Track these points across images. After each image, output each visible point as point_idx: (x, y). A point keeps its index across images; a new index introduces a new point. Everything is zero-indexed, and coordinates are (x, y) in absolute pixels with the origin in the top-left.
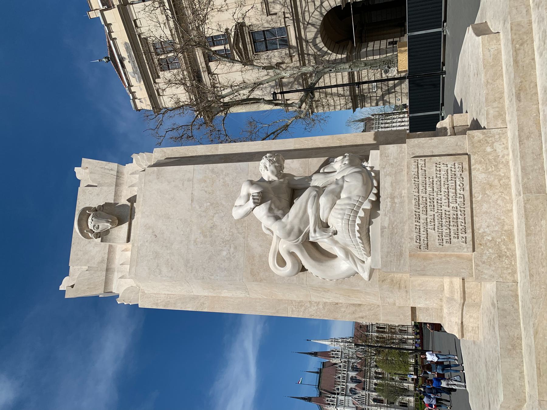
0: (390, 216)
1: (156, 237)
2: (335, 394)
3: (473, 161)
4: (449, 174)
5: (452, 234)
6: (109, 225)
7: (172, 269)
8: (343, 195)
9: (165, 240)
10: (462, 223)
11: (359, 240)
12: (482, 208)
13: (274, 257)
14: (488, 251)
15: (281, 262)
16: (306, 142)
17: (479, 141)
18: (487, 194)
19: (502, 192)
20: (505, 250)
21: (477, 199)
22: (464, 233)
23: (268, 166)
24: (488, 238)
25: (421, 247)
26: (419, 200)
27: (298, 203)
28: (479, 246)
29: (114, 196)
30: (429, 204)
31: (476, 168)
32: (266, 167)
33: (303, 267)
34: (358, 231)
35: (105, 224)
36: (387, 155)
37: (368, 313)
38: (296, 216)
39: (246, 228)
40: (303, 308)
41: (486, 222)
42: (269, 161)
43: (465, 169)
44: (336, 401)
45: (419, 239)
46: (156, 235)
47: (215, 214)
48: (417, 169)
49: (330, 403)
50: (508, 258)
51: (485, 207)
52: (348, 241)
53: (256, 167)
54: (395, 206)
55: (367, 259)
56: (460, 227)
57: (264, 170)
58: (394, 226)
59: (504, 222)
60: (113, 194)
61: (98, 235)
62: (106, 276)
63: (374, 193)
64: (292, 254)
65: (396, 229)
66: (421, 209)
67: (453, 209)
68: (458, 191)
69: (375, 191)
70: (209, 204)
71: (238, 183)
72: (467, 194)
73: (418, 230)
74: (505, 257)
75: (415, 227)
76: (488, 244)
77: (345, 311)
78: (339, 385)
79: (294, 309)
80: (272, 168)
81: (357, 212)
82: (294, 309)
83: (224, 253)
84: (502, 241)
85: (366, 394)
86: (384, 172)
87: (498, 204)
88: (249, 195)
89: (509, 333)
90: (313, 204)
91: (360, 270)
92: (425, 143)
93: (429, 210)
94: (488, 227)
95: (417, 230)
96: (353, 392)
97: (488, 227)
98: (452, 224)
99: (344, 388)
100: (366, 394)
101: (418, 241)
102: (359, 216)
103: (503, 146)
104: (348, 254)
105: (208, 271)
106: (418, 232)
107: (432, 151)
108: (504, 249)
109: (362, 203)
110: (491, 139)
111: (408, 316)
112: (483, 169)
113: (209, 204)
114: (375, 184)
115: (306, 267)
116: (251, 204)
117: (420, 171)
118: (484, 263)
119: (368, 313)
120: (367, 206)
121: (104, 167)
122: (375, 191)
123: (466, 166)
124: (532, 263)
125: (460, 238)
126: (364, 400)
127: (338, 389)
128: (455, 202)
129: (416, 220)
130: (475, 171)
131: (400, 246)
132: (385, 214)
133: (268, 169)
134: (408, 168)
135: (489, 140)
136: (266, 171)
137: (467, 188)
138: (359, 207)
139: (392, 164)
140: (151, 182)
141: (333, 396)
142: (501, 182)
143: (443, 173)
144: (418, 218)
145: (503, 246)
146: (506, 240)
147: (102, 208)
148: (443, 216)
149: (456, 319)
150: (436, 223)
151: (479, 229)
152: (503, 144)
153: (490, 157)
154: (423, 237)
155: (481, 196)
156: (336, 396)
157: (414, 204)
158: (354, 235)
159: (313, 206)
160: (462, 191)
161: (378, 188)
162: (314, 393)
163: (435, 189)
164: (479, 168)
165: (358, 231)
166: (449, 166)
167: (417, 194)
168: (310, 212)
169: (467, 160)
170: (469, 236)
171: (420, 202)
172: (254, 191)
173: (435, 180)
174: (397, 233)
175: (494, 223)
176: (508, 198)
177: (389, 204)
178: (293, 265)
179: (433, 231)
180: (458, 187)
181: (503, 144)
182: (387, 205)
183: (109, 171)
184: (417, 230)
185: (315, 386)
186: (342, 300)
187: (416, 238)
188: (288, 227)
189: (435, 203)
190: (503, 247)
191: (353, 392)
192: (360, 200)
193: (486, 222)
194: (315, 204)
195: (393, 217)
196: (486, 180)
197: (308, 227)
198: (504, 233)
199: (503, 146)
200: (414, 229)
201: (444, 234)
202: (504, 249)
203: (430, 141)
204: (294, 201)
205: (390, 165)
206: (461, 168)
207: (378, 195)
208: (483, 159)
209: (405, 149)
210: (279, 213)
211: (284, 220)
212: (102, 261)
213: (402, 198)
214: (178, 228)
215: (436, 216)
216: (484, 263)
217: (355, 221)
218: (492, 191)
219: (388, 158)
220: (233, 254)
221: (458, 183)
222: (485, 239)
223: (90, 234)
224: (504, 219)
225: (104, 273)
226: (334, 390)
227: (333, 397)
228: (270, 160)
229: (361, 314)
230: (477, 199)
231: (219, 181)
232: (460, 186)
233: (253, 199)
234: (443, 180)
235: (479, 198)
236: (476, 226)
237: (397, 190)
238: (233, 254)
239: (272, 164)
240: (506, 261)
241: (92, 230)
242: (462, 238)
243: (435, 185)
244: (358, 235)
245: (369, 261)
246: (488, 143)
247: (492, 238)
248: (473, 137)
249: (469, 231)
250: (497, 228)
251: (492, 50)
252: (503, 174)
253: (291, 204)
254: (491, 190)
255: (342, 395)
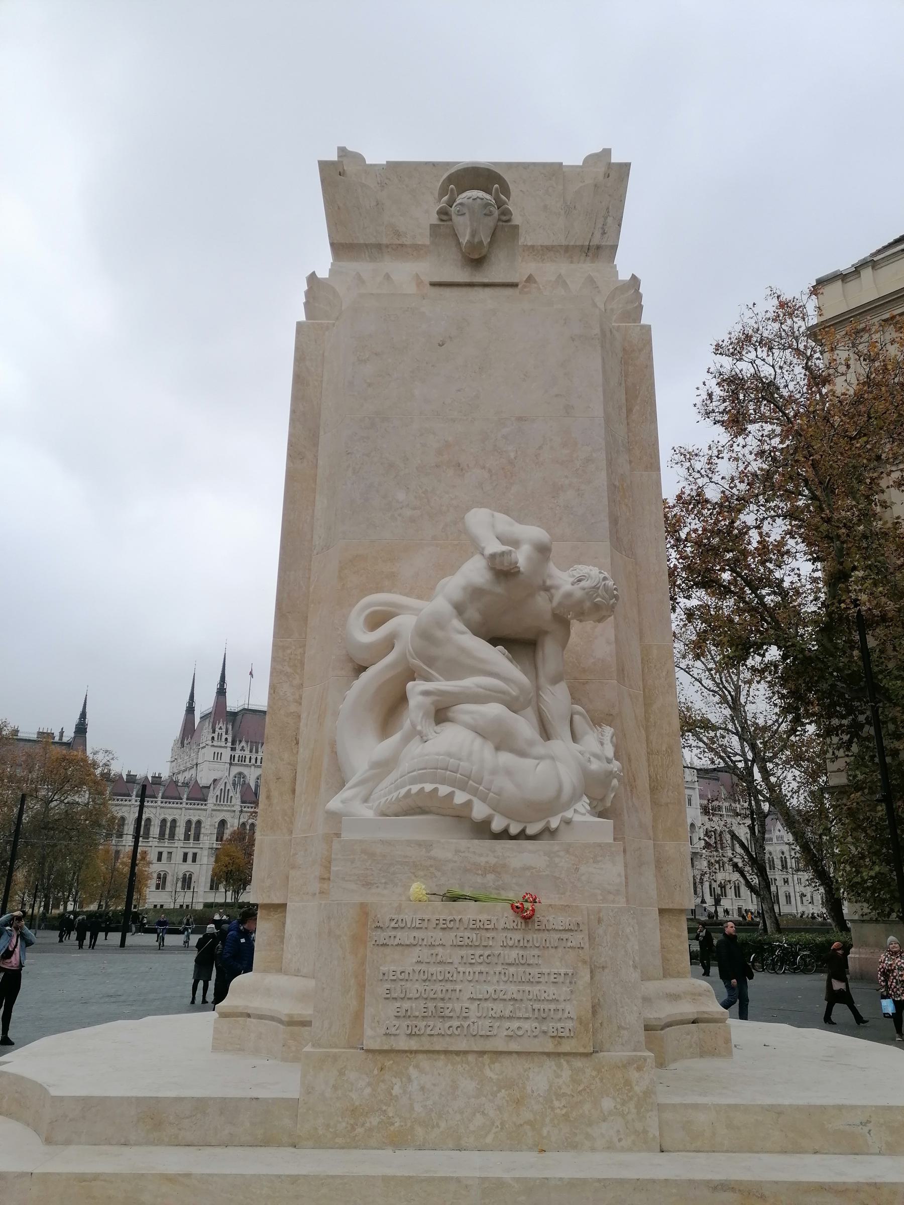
0: (455, 862)
1: (440, 345)
2: (233, 743)
3: (578, 1063)
4: (546, 1006)
5: (406, 1005)
6: (467, 238)
7: (370, 385)
8: (505, 758)
9: (433, 366)
10: (430, 1028)
11: (403, 791)
12: (466, 1079)
13: (380, 604)
14: (369, 1084)
15: (376, 620)
16: (664, 674)
17: (628, 1083)
18: (499, 1091)
19: (502, 1128)
20: (368, 1125)
21: (487, 1067)
22: (409, 1032)
23: (582, 584)
24: (396, 1088)
25: (379, 932)
26: (487, 929)
27: (496, 656)
28: (380, 1066)
29: (541, 246)
30: (479, 952)
31: (562, 1070)
32: (580, 581)
33: (364, 669)
34: (423, 788)
35: (469, 228)
36: (599, 859)
37: (278, 808)
38: (463, 650)
39: (456, 542)
40: (289, 670)
41: (434, 1085)
42: (594, 587)
43: (559, 1043)
44: (219, 744)
45: (397, 926)
46: (443, 345)
47: (490, 471)
48: (561, 928)
49: (217, 733)
50: (349, 1128)
51: (468, 1085)
52: (405, 765)
53: (596, 558)
54: (478, 874)
55: (370, 808)
56: (422, 1024)
57: (574, 576)
58: (432, 870)
59: (433, 1127)
60: (547, 243)
61: (444, 214)
62: (366, 245)
63: (508, 826)
64: (389, 644)
65: (425, 875)
66: (467, 934)
67: (464, 1010)
68: (507, 1024)
69: (514, 830)
70: (512, 455)
71: (560, 519)
72: (499, 1044)
73: (418, 926)
74: (352, 1122)
75: (426, 917)
76: (383, 1086)
77: (282, 760)
78: (251, 751)
79: (289, 651)
80: (579, 594)
81: (463, 787)
82: (289, 651)
83: (401, 496)
84: (389, 1118)
85: (233, 806)
86: (558, 851)
87: (474, 1115)
88: (515, 543)
89: (187, 1118)
90: (486, 689)
91: (346, 793)
92: (626, 951)
93: (463, 952)
94: (422, 1089)
95: (418, 922)
96: (236, 779)
97: (422, 1089)
98: (431, 1005)
99: (245, 761)
100: (233, 806)
101: (393, 924)
102: (453, 792)
103: (615, 1139)
104: (384, 766)
105: (362, 464)
106: (413, 926)
107: (606, 967)
108: (370, 1123)
109: (484, 799)
110: (634, 1111)
111: (269, 897)
112: (560, 1088)
113: (512, 455)
114: (531, 830)
115: (364, 676)
116: (494, 547)
117: (556, 936)
118: (341, 1073)
119: (278, 808)
120: (480, 811)
121: (610, 214)
122: (514, 830)
123: (566, 1047)
124: (323, 1184)
125: (396, 1023)
126: (222, 803)
127: (243, 749)
128: (479, 1015)
129: (441, 921)
130: (555, 1068)
131: (385, 883)
132: (460, 851)
133: (576, 586)
134: (565, 908)
135: (632, 1105)
136: (572, 580)
137: (514, 1046)
138: (475, 792)
139: (577, 870)
140: (565, 323)
141: (230, 740)
142: (527, 1127)
143: (552, 990)
144: (445, 926)
145: (378, 1120)
146: (392, 1128)
147: (504, 218)
148: (449, 986)
149: (257, 1004)
150: (433, 969)
151: (417, 1067)
152: (620, 1140)
153: (587, 1107)
154: (404, 937)
155: (494, 1077)
156: (229, 744)
157: (481, 917)
158: (414, 781)
159: (484, 688)
160: (506, 1033)
161: (522, 835)
162: (233, 703)
163: (512, 970)
164: (561, 1076)
165: (423, 788)
166: (568, 1007)
167: (502, 925)
168: (470, 683)
169: (582, 1050)
170: (403, 1044)
171: (484, 933)
172: (522, 557)
173: (534, 971)
174: (415, 876)
175: (429, 1103)
176: (489, 1139)
177: (482, 860)
178: (369, 647)
179: (415, 960)
180: (515, 1024)
181: (620, 1140)
182: (481, 855)
183: (600, 226)
184: (418, 922)
185: (247, 702)
186: (304, 753)
187: (400, 921)
188: (440, 634)
189: (478, 969)
190: (374, 1120)
191: (236, 779)
192: (491, 794)
193: (434, 1085)
194: (488, 692)
195: (452, 869)
196: (533, 1091)
197: (441, 678)
198: (406, 1125)
199: (615, 1139)
200: (419, 916)
201: (409, 985)
202: (370, 1123)
203: (631, 963)
204: (500, 647)
205: (573, 864)
206: (562, 1034)
207: (504, 835)
208: (585, 1090)
209: (613, 902)
210: (473, 614)
211: (457, 624)
212: (398, 234)
213: (497, 892)
214: (459, 391)
215: (448, 968)
216: (341, 1073)
217: (443, 781)
218: (505, 1104)
219: (591, 861)
220: (400, 515)
221: (527, 1025)
222: (394, 1080)
223: (446, 198)
224: (438, 1126)
225: (373, 240)
226: (240, 741)
227: (226, 739)
228: (596, 588)
229: (275, 794)
230: (487, 1067)
231: (566, 477)
232: (519, 1028)
233: (503, 554)
234: (535, 989)
235: (488, 1073)
236: (424, 1062)
237: (514, 881)
238: (400, 515)
239: (587, 593)
240: (344, 1124)
241: (455, 201)
242: (396, 1027)
243: (521, 969)
244: (415, 788)
245: (367, 813)
246: (624, 1103)
247: (396, 1096)
248: (639, 1069)
249: (413, 1044)
250: (418, 1108)
251: (866, 1129)
252: (545, 1132)
253: (494, 641)
254: (507, 1101)
255: (232, 758)
